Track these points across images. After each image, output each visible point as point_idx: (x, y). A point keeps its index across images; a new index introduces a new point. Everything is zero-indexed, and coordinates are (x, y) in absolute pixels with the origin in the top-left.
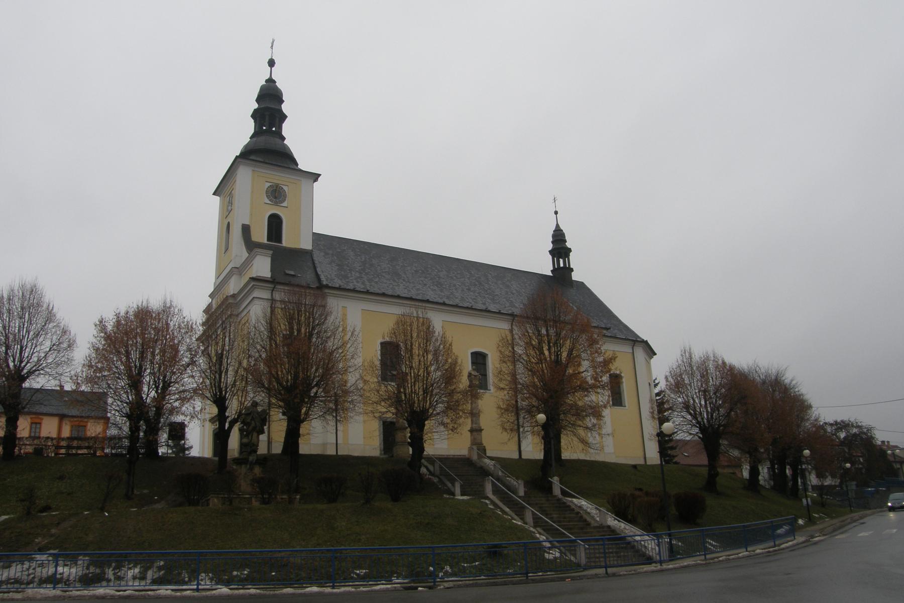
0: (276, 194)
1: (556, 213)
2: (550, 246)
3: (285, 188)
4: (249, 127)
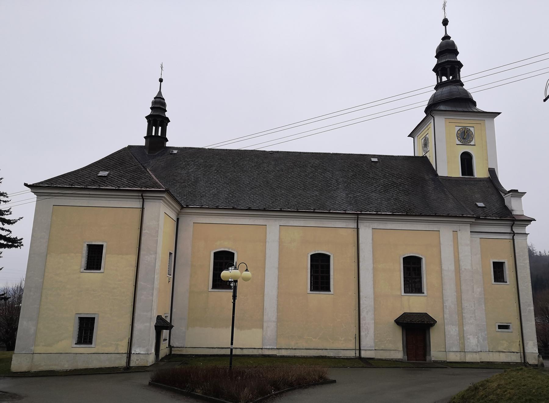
0: (465, 136)
1: (161, 80)
2: (149, 112)
3: (472, 129)
4: (433, 79)
